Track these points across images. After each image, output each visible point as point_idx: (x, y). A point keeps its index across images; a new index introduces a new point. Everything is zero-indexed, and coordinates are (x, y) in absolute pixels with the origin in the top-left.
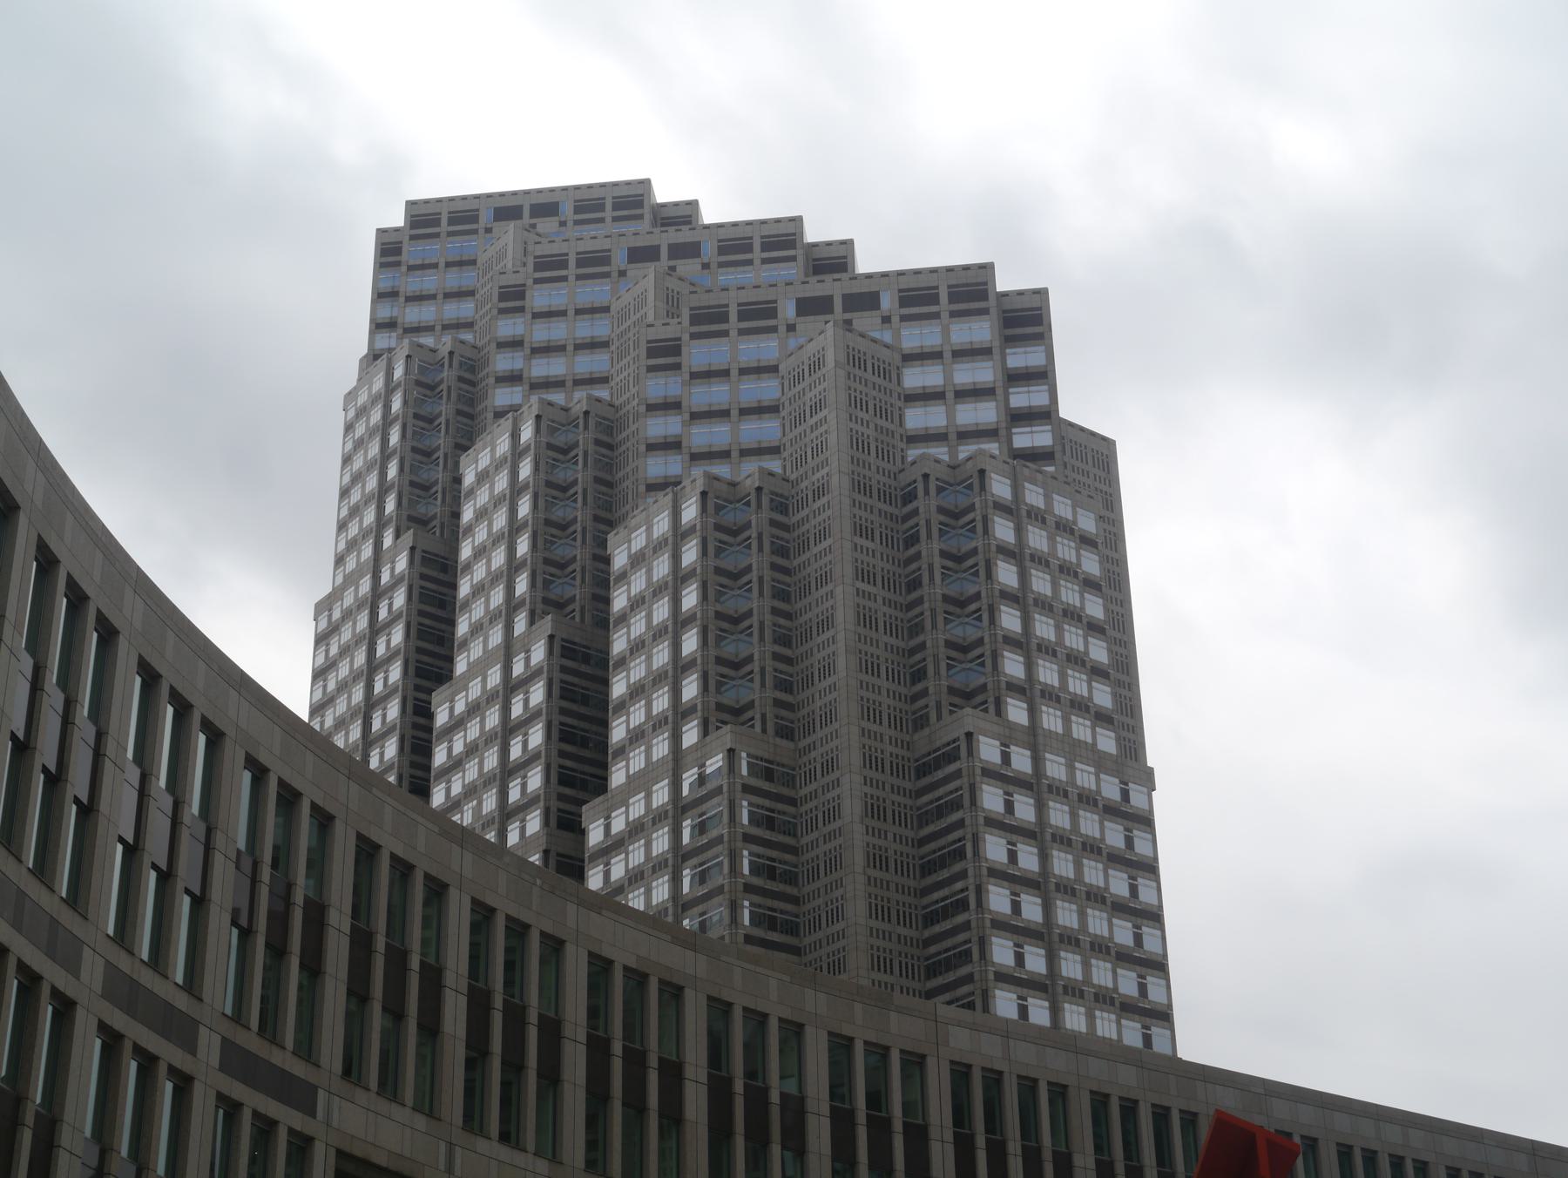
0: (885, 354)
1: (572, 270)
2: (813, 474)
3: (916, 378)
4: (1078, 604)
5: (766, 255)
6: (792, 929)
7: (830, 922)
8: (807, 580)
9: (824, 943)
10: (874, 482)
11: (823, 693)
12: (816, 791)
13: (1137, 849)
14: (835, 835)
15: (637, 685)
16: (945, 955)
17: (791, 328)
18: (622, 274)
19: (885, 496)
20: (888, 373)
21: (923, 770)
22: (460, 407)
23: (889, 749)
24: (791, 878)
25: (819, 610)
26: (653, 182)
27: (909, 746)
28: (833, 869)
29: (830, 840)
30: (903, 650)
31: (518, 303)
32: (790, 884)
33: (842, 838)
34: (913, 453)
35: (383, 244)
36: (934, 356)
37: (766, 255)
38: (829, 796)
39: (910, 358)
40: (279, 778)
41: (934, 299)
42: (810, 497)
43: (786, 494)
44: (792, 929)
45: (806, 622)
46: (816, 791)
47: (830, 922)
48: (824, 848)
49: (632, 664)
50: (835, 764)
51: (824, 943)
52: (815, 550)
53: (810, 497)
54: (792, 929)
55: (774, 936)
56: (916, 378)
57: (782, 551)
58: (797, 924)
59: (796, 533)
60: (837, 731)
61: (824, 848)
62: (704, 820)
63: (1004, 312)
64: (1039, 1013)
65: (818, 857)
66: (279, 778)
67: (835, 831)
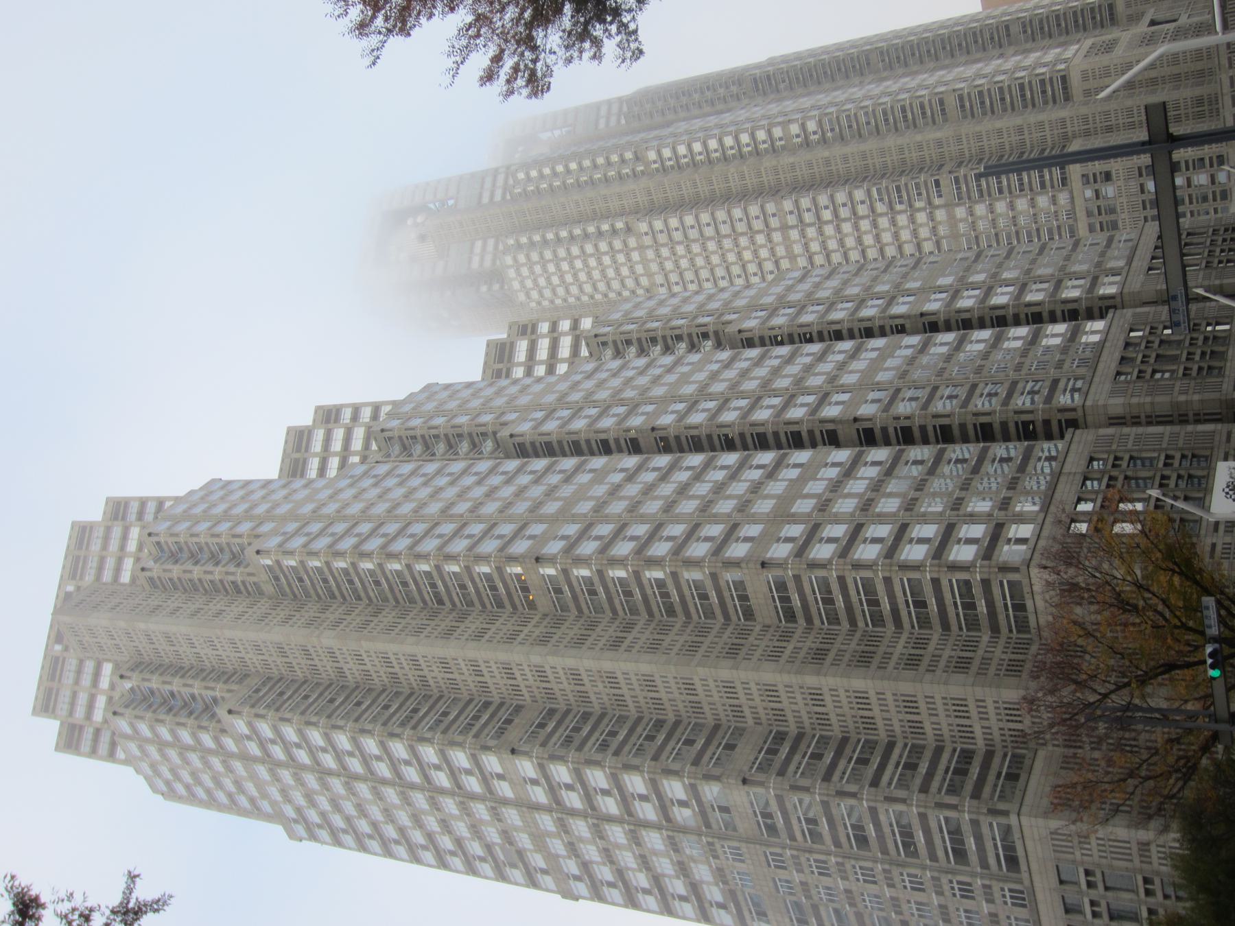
3: (107, 576)
4: (867, 482)
6: (966, 757)
7: (654, 689)
8: (611, 697)
9: (986, 723)
10: (614, 634)
12: (838, 715)
13: (843, 460)
14: (933, 709)
15: (677, 868)
16: (960, 608)
21: (790, 616)
23: (853, 645)
24: (917, 750)
27: (766, 627)
30: (991, 637)
32: (922, 753)
33: (695, 677)
38: (844, 701)
43: (541, 708)
44: (870, 745)
46: (983, 727)
47: (654, 689)
48: (942, 718)
49: (622, 864)
50: (910, 699)
51: (986, 723)
54: (966, 757)
55: (923, 768)
56: (107, 576)
58: (963, 751)
60: (786, 686)
61: (942, 718)
62: (718, 807)
63: (91, 528)
64: (754, 530)
65: (949, 725)
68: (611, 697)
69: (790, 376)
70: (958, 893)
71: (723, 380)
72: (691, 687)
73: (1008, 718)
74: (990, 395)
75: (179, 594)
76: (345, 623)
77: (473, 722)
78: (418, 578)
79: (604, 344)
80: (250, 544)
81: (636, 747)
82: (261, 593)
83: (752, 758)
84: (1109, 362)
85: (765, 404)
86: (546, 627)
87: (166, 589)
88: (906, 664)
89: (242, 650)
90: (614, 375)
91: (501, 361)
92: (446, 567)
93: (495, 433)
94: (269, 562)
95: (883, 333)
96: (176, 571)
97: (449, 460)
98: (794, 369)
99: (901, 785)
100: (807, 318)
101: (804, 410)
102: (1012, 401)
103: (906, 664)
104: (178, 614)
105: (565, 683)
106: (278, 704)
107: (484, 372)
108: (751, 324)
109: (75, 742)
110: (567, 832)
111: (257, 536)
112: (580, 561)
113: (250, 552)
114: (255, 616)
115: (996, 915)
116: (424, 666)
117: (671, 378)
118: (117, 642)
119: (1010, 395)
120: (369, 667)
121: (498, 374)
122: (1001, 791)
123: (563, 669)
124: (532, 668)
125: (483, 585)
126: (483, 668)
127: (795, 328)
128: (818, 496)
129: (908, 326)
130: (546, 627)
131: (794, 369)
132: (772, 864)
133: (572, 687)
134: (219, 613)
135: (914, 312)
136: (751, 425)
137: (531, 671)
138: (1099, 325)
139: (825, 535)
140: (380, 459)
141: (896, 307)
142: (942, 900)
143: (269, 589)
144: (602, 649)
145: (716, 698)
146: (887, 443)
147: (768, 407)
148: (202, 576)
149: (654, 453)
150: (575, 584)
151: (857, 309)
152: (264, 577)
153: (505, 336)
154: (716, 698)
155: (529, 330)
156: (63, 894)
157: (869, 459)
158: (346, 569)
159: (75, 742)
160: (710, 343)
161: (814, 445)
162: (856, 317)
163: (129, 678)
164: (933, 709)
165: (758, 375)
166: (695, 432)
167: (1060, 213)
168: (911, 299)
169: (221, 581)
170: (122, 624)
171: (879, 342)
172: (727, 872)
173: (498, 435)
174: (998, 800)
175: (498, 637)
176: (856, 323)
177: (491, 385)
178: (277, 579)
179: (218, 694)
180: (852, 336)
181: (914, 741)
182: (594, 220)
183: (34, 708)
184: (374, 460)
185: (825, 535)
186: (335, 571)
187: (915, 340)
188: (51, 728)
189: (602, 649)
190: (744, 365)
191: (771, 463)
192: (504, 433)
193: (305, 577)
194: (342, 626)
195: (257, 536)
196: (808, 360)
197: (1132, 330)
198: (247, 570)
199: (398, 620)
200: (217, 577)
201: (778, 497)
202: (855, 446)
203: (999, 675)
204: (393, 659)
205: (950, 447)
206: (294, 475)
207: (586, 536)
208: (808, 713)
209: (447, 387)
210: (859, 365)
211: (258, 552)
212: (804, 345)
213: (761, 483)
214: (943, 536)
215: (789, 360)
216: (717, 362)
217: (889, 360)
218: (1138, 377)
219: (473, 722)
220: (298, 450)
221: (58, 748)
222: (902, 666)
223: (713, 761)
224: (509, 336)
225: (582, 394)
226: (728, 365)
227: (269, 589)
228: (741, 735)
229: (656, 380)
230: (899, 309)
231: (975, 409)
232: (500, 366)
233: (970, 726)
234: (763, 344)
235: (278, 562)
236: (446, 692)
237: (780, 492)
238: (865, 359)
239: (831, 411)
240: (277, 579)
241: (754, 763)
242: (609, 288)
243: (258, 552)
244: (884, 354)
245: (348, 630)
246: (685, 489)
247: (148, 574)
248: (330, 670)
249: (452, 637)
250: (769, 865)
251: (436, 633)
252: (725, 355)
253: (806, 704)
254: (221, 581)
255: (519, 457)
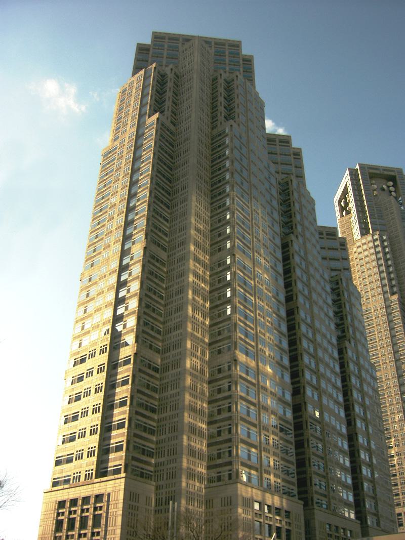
2: (181, 204)
11: (169, 462)
13: (286, 397)
14: (172, 418)
25: (179, 255)
28: (173, 431)
29: (180, 261)
31: (148, 52)
35: (139, 47)
40: (55, 466)
41: (179, 40)
42: (173, 311)
45: (165, 383)
52: (174, 334)
53: (173, 311)
59: (168, 307)
60: (174, 491)
66: (55, 466)
67: (173, 394)
68: (171, 309)
69: (324, 357)
71: (322, 340)
72: (178, 310)
73: (170, 450)
74: (319, 465)
75: (209, 201)
76: (201, 168)
77: (158, 229)
78: (223, 200)
79: (338, 283)
80: (235, 122)
81: (149, 304)
82: (212, 129)
83: (146, 357)
84: (335, 521)
85: (306, 302)
86: (203, 245)
87: (212, 123)
88: (191, 427)
89: (182, 192)
90: (323, 288)
91: (327, 234)
92: (228, 173)
93: (293, 233)
94: (227, 131)
95: (347, 416)
96: (221, 90)
97: (278, 200)
98: (328, 374)
99: (136, 425)
100: (351, 366)
101: (309, 379)
102: (316, 476)
103: (191, 427)
104: (202, 83)
105: (174, 322)
106: (163, 140)
107: (321, 227)
108: (350, 353)
109: (142, 52)
110: (110, 274)
111: (239, 125)
113: (231, 122)
114: (202, 116)
116: (183, 205)
117: (322, 315)
118: (187, 66)
119: (319, 475)
120: (181, 180)
121: (321, 233)
122: (135, 470)
123: (184, 269)
124: (181, 305)
125: (221, 190)
126: (183, 232)
127: (351, 402)
129: (350, 427)
130: (203, 245)
131: (328, 374)
132: (100, 367)
134: (203, 110)
135: (357, 430)
136: (301, 354)
137: (179, 322)
138: (353, 516)
140: (278, 180)
141: (354, 378)
143: (215, 132)
144: (193, 287)
145: (174, 304)
146: (295, 418)
147: (309, 346)
148: (219, 92)
149: (286, 308)
151: (358, 403)
152: (220, 129)
153: (340, 236)
154: (173, 340)
155: (343, 247)
157: (287, 410)
158: (226, 191)
159: (142, 52)
160: (340, 334)
161: (292, 384)
162: (354, 402)
163: (171, 72)
164: (172, 418)
165: (327, 372)
166: (297, 327)
167: (396, 433)
168: (364, 429)
170: (195, 67)
171: (342, 414)
172: (108, 249)
173: (292, 234)
174: (134, 445)
175: (198, 210)
176: (351, 402)
177: (315, 230)
178: (220, 135)
179: (166, 113)
180: (345, 401)
181: (156, 431)
182: (397, 277)
183: (156, 32)
184: (277, 177)
186: (224, 161)
187: (344, 430)
188: (148, 41)
189: (193, 287)
190: (330, 350)
191: (285, 399)
192: (293, 237)
193: (221, 148)
194: (199, 166)
195: (239, 125)
196: (333, 380)
197: (351, 531)
198: (223, 122)
199: (202, 219)
202: (293, 403)
203: (187, 493)
204: (185, 190)
205: (293, 447)
206: (268, 140)
208: (168, 383)
209: (314, 210)
210: (332, 405)
211: (231, 126)
212: (340, 378)
214: (251, 443)
215: (333, 372)
216: (331, 337)
217: (334, 419)
218: (328, 534)
219: (158, 229)
220: (280, 142)
221: (138, 44)
222: (191, 425)
223: (145, 340)
224: (340, 238)
225: (313, 273)
226: (330, 342)
227: (215, 132)
228: (155, 371)
229: (321, 308)
230: (359, 423)
231: (310, 439)
232: (325, 234)
233: (162, 505)
234: (340, 359)
235: (227, 135)
236: (176, 153)
238: (334, 407)
239: (309, 392)
240: (220, 135)
241: (144, 358)
242: (359, 254)
243: (231, 126)
244: (337, 417)
245: (198, 169)
247: (219, 77)
248: (177, 187)
249: (196, 217)
250: (99, 366)
251: (198, 210)
252: (334, 341)
253: (171, 381)
255: (282, 245)
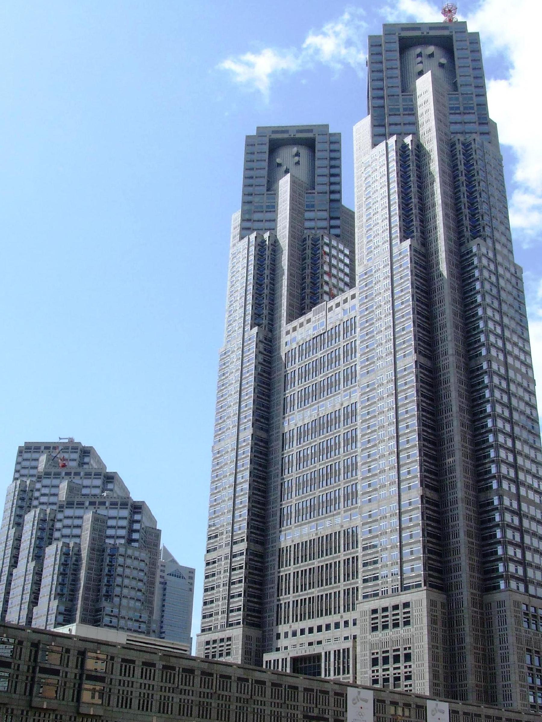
0: (104, 518)
1: (119, 506)
3: (111, 523)
5: (72, 451)
17: (87, 508)
18: (63, 478)
19: (98, 551)
20: (104, 522)
22: (258, 407)
26: (248, 135)
34: (108, 541)
36: (115, 518)
37: (72, 451)
39: (110, 518)
56: (111, 523)
57: (386, 660)
70: (383, 589)
92: (481, 308)
112: (484, 310)
115: (385, 487)
128: (523, 451)
133: (436, 287)
139: (506, 424)
142: (380, 584)
150: (475, 309)
156: (165, 628)
169: (461, 202)
185: (506, 424)
200: (462, 200)
201: (514, 365)
207: (500, 378)
213: (528, 443)
237: (529, 497)
246: (527, 458)
254: (461, 202)
